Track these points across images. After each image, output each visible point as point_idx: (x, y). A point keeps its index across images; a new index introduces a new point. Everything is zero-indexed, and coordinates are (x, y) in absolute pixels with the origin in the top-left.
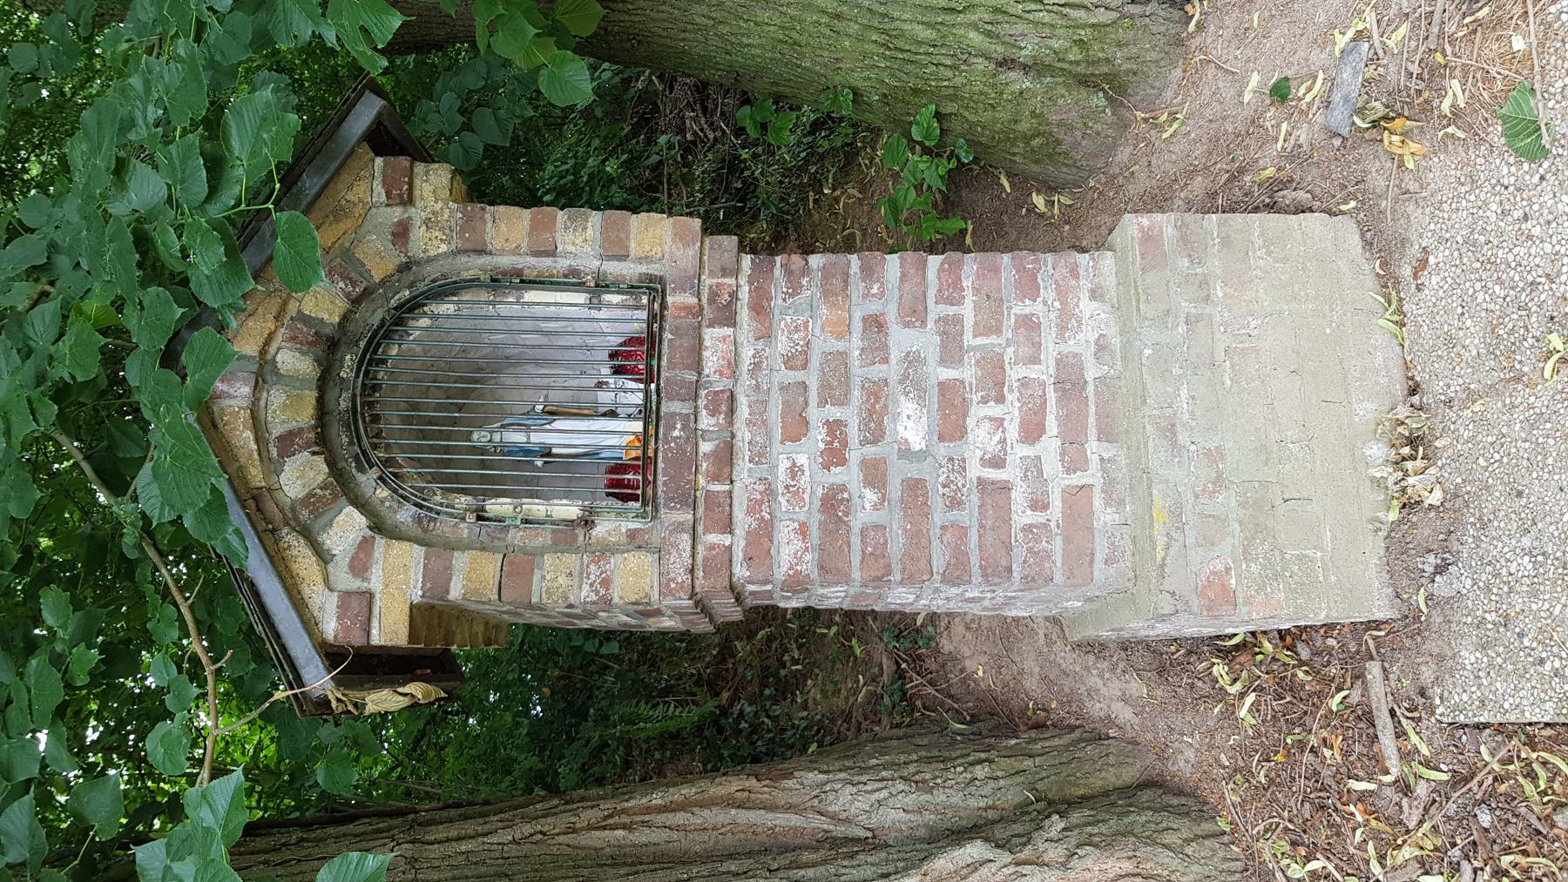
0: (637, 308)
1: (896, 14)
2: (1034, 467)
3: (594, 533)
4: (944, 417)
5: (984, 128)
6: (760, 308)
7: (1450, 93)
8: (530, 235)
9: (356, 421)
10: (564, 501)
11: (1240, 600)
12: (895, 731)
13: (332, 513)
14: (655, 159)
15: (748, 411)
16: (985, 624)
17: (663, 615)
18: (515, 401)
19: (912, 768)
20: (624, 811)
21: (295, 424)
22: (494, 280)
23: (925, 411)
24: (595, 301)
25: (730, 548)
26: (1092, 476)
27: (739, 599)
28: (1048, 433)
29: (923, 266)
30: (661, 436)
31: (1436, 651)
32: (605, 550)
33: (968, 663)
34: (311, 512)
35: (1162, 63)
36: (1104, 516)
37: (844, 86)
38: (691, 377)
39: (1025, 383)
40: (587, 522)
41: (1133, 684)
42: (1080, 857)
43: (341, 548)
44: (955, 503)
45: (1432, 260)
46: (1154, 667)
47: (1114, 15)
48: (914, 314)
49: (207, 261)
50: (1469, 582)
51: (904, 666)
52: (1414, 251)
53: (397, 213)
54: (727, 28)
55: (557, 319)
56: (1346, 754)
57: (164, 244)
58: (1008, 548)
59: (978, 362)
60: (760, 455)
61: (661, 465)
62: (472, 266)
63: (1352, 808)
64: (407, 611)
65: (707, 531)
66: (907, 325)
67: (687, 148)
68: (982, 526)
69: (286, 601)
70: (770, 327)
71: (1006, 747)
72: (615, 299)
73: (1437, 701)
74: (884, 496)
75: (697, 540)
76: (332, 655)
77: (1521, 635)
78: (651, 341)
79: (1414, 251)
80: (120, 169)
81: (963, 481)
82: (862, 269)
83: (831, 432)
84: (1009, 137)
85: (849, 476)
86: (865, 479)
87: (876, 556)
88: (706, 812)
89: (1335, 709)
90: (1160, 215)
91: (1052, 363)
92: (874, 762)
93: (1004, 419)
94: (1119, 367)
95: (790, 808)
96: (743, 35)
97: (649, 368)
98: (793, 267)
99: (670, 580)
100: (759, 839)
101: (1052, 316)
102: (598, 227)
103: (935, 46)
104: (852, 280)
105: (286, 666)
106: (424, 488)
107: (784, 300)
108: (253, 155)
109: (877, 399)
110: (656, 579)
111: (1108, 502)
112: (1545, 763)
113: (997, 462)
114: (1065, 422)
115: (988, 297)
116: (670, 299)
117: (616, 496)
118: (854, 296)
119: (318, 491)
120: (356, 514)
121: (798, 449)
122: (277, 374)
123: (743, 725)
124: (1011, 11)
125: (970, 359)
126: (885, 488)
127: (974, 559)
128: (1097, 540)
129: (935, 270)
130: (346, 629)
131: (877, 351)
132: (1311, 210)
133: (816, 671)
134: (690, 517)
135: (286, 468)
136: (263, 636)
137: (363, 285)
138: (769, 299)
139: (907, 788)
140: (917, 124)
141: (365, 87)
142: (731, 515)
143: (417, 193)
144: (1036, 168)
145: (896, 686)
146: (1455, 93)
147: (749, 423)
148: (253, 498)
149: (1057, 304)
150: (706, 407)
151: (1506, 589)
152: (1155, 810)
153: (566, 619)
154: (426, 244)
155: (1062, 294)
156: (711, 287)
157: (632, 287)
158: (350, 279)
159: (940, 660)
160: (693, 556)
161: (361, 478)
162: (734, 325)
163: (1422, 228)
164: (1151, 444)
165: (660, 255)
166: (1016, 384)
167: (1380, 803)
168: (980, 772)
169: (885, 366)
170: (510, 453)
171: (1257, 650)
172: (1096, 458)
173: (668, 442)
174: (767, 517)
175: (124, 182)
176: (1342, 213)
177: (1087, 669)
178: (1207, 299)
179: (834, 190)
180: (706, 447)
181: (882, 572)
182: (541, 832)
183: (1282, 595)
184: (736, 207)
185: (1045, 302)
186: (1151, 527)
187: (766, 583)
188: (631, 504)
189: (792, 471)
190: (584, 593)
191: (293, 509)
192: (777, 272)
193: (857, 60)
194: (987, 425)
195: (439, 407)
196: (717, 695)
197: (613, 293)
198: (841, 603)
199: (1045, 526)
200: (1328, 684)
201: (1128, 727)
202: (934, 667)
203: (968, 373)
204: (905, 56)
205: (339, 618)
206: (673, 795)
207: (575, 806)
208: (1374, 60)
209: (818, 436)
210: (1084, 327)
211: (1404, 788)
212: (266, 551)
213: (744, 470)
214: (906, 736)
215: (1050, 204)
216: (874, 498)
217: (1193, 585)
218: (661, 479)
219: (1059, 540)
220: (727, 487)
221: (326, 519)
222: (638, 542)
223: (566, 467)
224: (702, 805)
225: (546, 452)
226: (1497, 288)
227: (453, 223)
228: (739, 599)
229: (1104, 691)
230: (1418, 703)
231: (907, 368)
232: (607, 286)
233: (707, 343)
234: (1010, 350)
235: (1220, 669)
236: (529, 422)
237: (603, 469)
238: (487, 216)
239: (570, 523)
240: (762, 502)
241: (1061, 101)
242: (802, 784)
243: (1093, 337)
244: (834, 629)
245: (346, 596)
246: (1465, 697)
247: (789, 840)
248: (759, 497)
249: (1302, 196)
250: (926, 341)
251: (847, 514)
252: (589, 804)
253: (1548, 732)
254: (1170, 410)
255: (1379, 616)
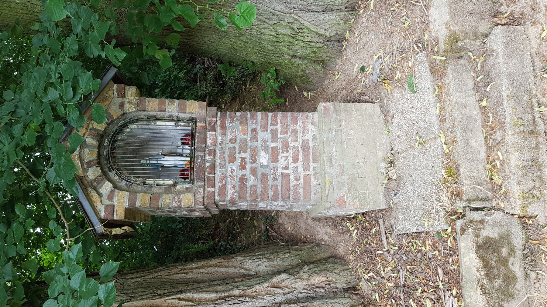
0: (189, 126)
1: (263, 42)
2: (296, 170)
3: (176, 188)
4: (273, 156)
5: (289, 74)
6: (223, 127)
7: (397, 75)
8: (158, 106)
9: (109, 158)
10: (168, 180)
11: (347, 204)
12: (265, 245)
13: (103, 183)
14: (195, 71)
15: (219, 154)
16: (291, 214)
17: (196, 211)
18: (153, 152)
19: (268, 255)
20: (185, 269)
21: (91, 158)
22: (148, 119)
23: (267, 155)
24: (177, 124)
26: (311, 172)
27: (217, 206)
28: (300, 161)
29: (267, 116)
30: (195, 161)
31: (394, 216)
32: (179, 193)
33: (286, 226)
35: (336, 58)
36: (314, 182)
37: (249, 61)
38: (204, 145)
40: (174, 185)
41: (328, 229)
42: (312, 277)
43: (105, 193)
44: (275, 179)
45: (395, 116)
46: (333, 224)
47: (322, 45)
48: (265, 128)
49: (73, 115)
50: (401, 198)
51: (268, 227)
52: (391, 114)
53: (120, 100)
54: (215, 44)
55: (166, 129)
56: (376, 244)
57: (60, 110)
58: (289, 191)
59: (282, 141)
60: (223, 167)
61: (195, 170)
62: (142, 114)
63: (377, 258)
66: (263, 131)
67: (205, 69)
68: (282, 185)
69: (90, 207)
71: (294, 248)
72: (182, 124)
73: (395, 229)
75: (205, 190)
76: (102, 221)
77: (411, 211)
78: (192, 135)
79: (391, 114)
80: (45, 90)
81: (277, 173)
83: (242, 160)
84: (296, 76)
85: (247, 172)
86: (251, 173)
87: (254, 193)
88: (209, 269)
89: (374, 233)
90: (329, 103)
91: (301, 142)
92: (258, 254)
93: (288, 157)
94: (318, 143)
95: (233, 267)
96: (220, 46)
97: (192, 143)
98: (232, 115)
99: (197, 201)
100: (224, 275)
101: (301, 129)
103: (274, 51)
104: (248, 119)
105: (91, 225)
106: (128, 176)
107: (229, 124)
108: (86, 88)
109: (255, 151)
110: (194, 200)
111: (315, 179)
112: (415, 242)
113: (286, 168)
114: (304, 157)
115: (284, 124)
116: (198, 124)
117: (183, 178)
118: (249, 123)
119: (98, 177)
120: (109, 183)
121: (233, 165)
122: (86, 145)
123: (222, 248)
124: (294, 43)
125: (279, 140)
126: (256, 175)
127: (280, 194)
128: (312, 189)
129: (270, 116)
130: (107, 215)
131: (255, 138)
132: (368, 102)
133: (244, 231)
134: (203, 183)
135: (89, 171)
136: (84, 217)
137: (111, 120)
138: (225, 124)
139: (266, 260)
140: (270, 72)
141: (112, 65)
143: (126, 94)
144: (303, 85)
145: (265, 233)
146: (398, 75)
147: (220, 158)
148: (80, 179)
149: (302, 126)
150: (208, 154)
151: (408, 200)
152: (333, 263)
153: (168, 213)
154: (129, 108)
155: (304, 124)
156: (209, 121)
157: (187, 121)
159: (278, 225)
160: (204, 194)
161: (110, 173)
162: (216, 131)
163: (393, 108)
164: (325, 163)
165: (195, 112)
167: (384, 256)
168: (287, 255)
169: (257, 143)
170: (152, 166)
171: (357, 218)
172: (312, 167)
175: (47, 93)
176: (376, 103)
177: (317, 226)
178: (340, 125)
179: (250, 86)
180: (207, 165)
181: (256, 198)
182: (160, 275)
183: (358, 202)
184: (220, 89)
185: (299, 126)
186: (325, 185)
187: (224, 201)
188: (187, 180)
190: (174, 204)
191: (91, 182)
192: (228, 116)
193: (252, 54)
194: (284, 158)
195: (131, 154)
196: (214, 240)
197: (182, 122)
198: (247, 208)
199: (299, 185)
200: (372, 225)
201: (327, 241)
202: (277, 227)
203: (279, 144)
204: (266, 53)
205: (105, 212)
206: (199, 264)
207: (170, 268)
208: (382, 64)
209: (239, 161)
210: (309, 132)
211: (388, 251)
212: (84, 194)
213: (218, 171)
214: (267, 247)
215: (308, 95)
216: (254, 178)
217: (335, 200)
218: (195, 173)
219: (302, 189)
221: (101, 185)
222: (189, 190)
223: (168, 170)
224: (207, 267)
225: (162, 166)
226: (407, 124)
227: (136, 103)
228: (217, 206)
229: (321, 232)
230: (390, 230)
231: (263, 143)
232: (180, 120)
233: (208, 136)
234: (290, 138)
235: (349, 224)
236: (157, 157)
237: (179, 171)
241: (309, 67)
243: (312, 135)
244: (249, 218)
245: (107, 206)
246: (400, 227)
247: (232, 276)
248: (222, 178)
249: (367, 98)
250: (267, 136)
251: (246, 182)
252: (174, 267)
253: (416, 235)
254: (330, 154)
255: (383, 208)
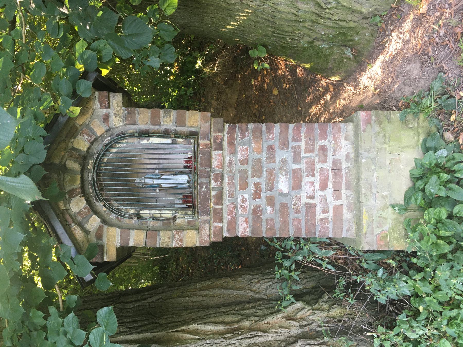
2: (324, 198)
6: (231, 143)
25: (222, 227)
29: (288, 127)
34: (81, 217)
39: (322, 169)
40: (174, 218)
48: (284, 144)
53: (105, 111)
59: (306, 162)
60: (232, 195)
64: (115, 250)
65: (214, 222)
66: (282, 149)
70: (235, 149)
72: (181, 140)
74: (274, 208)
82: (267, 129)
83: (256, 187)
85: (262, 202)
99: (202, 240)
101: (332, 146)
102: (175, 116)
107: (240, 140)
109: (271, 175)
110: (198, 239)
114: (335, 183)
118: (264, 139)
119: (83, 210)
120: (97, 218)
125: (304, 161)
126: (274, 206)
131: (271, 158)
134: (209, 218)
138: (234, 140)
142: (222, 216)
143: (111, 104)
147: (228, 184)
149: (333, 142)
150: (213, 179)
155: (335, 139)
156: (214, 136)
158: (90, 135)
165: (196, 126)
166: (319, 170)
173: (201, 193)
174: (234, 216)
180: (213, 193)
185: (329, 141)
189: (243, 200)
190: (174, 244)
192: (237, 129)
194: (309, 185)
195: (122, 170)
199: (327, 219)
203: (303, 166)
209: (252, 188)
210: (342, 150)
213: (226, 200)
220: (221, 207)
224: (214, 288)
233: (213, 156)
238: (136, 112)
239: (168, 219)
240: (233, 211)
242: (244, 279)
250: (287, 155)
